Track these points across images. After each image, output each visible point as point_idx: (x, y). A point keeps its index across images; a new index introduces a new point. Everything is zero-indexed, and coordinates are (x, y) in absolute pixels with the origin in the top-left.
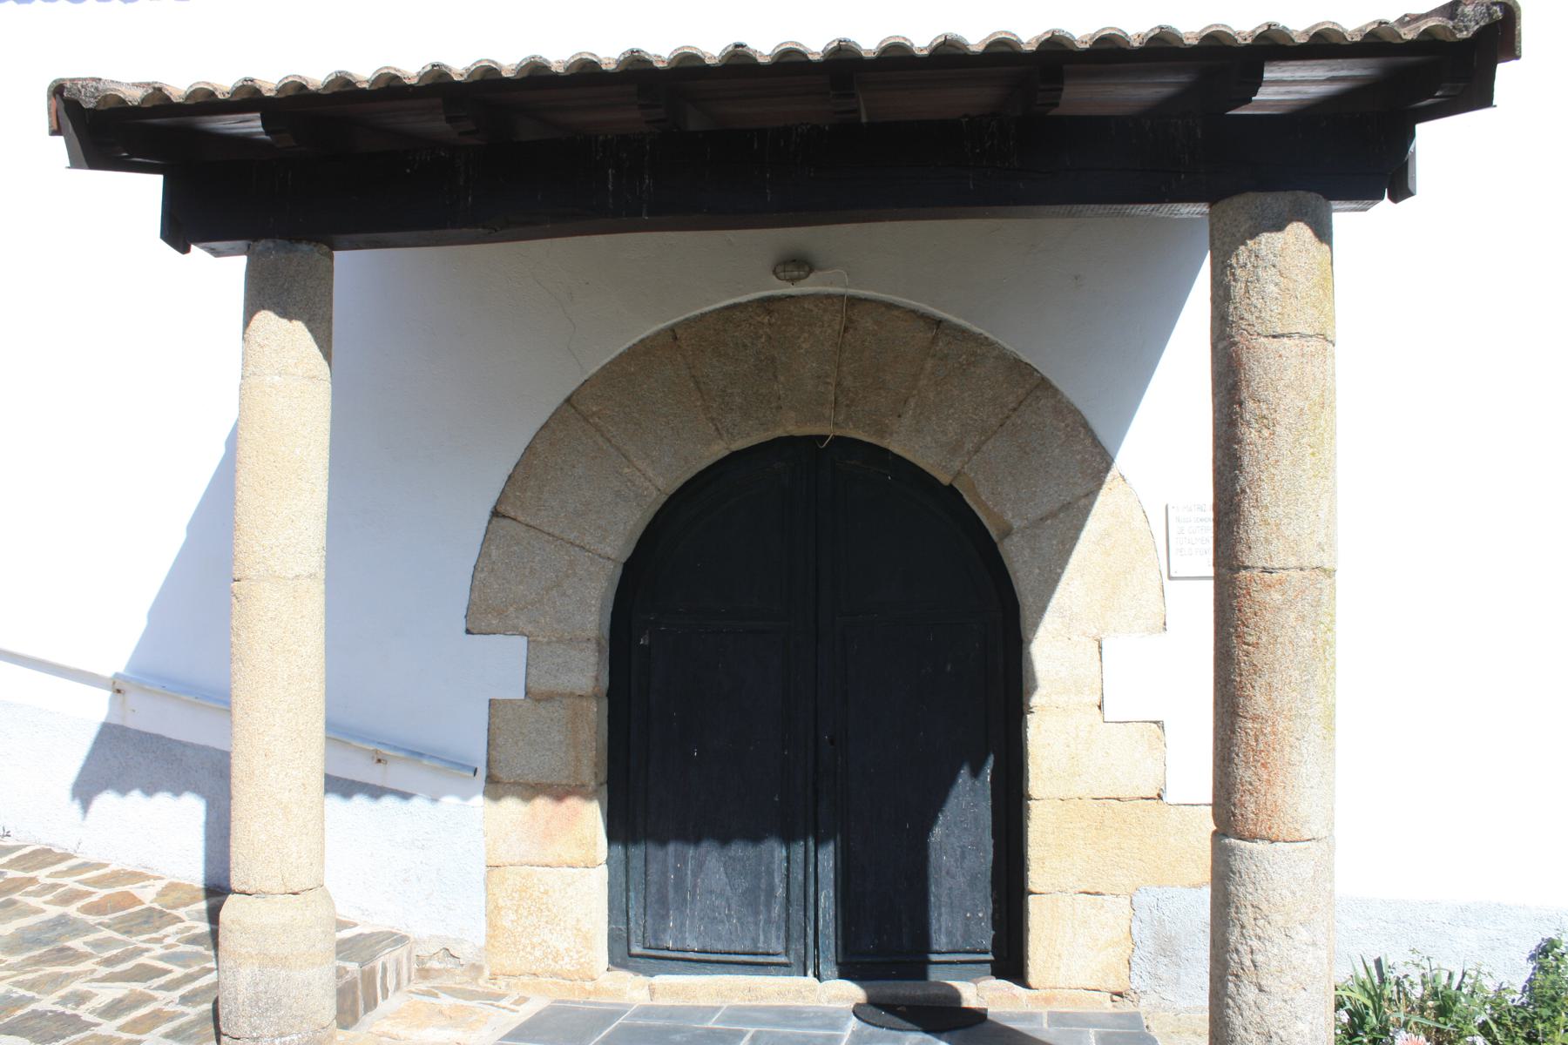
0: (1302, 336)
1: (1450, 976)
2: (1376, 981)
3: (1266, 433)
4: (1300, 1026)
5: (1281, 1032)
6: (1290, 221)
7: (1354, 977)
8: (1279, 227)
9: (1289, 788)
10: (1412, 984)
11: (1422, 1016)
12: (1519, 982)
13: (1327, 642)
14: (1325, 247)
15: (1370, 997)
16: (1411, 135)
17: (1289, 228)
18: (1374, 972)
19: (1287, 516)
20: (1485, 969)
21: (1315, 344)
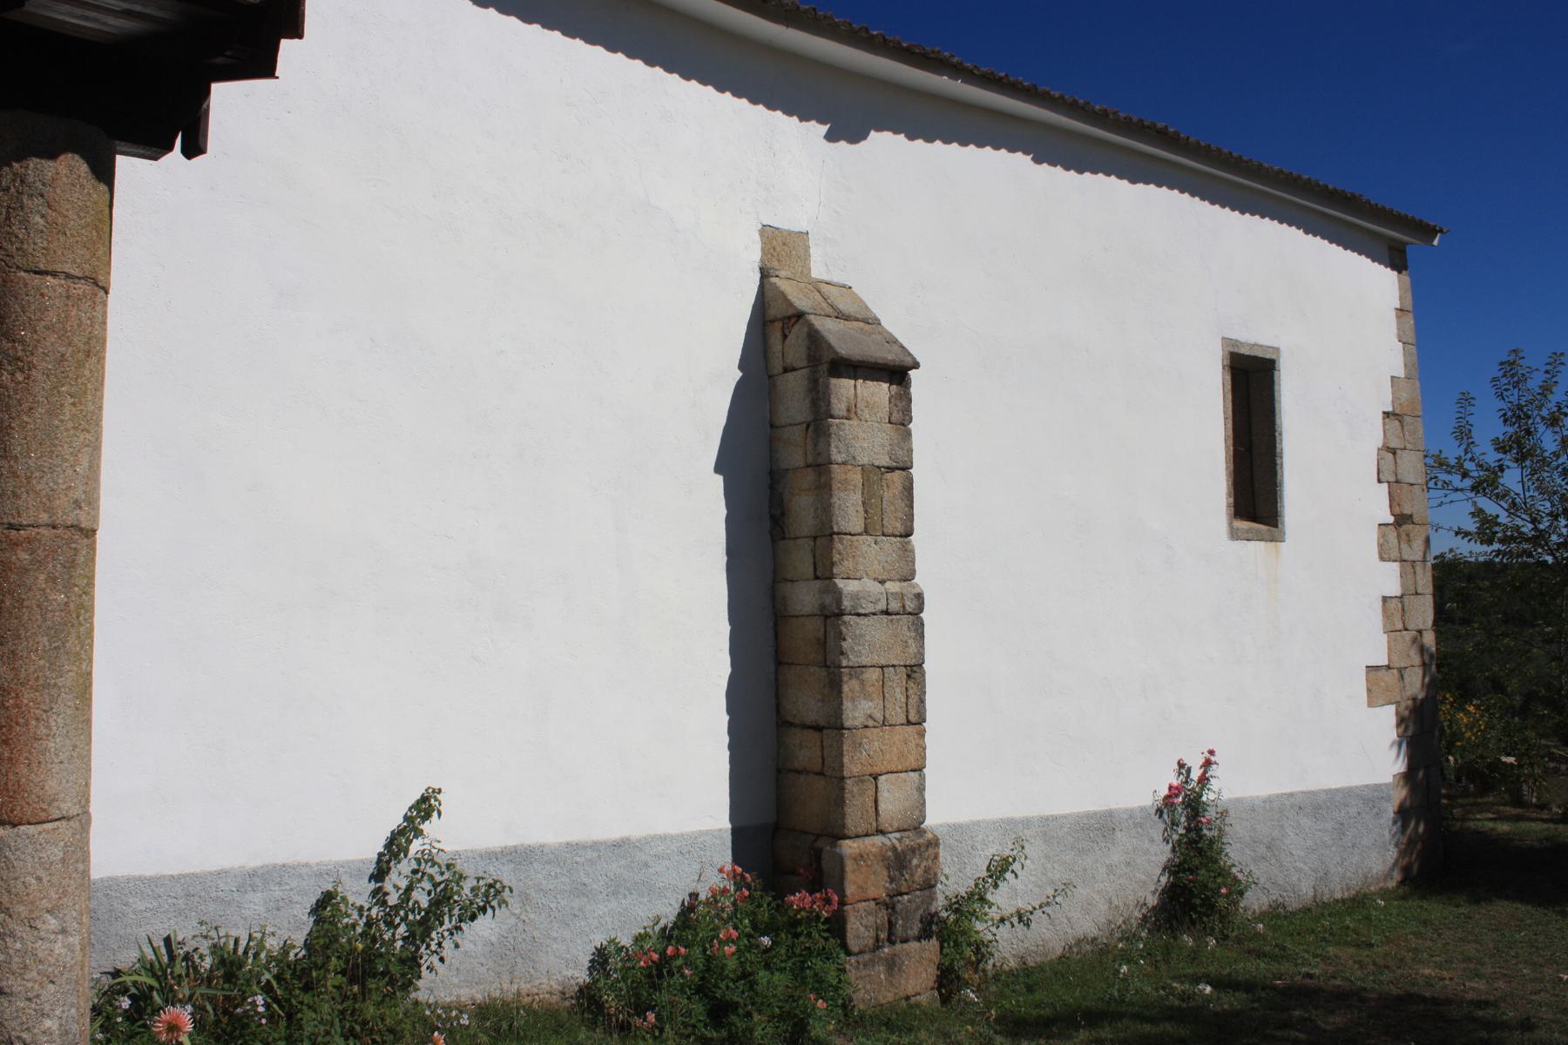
0: (68, 276)
1: (237, 941)
2: (165, 959)
3: (20, 377)
4: (48, 1023)
5: (25, 1035)
6: (65, 150)
7: (142, 960)
8: (52, 155)
9: (34, 765)
10: (202, 957)
11: (209, 986)
12: (299, 938)
13: (81, 606)
14: (103, 187)
15: (154, 975)
16: (208, 92)
17: (62, 157)
18: (163, 951)
19: (39, 468)
20: (269, 929)
21: (82, 288)
